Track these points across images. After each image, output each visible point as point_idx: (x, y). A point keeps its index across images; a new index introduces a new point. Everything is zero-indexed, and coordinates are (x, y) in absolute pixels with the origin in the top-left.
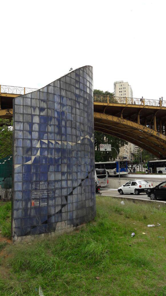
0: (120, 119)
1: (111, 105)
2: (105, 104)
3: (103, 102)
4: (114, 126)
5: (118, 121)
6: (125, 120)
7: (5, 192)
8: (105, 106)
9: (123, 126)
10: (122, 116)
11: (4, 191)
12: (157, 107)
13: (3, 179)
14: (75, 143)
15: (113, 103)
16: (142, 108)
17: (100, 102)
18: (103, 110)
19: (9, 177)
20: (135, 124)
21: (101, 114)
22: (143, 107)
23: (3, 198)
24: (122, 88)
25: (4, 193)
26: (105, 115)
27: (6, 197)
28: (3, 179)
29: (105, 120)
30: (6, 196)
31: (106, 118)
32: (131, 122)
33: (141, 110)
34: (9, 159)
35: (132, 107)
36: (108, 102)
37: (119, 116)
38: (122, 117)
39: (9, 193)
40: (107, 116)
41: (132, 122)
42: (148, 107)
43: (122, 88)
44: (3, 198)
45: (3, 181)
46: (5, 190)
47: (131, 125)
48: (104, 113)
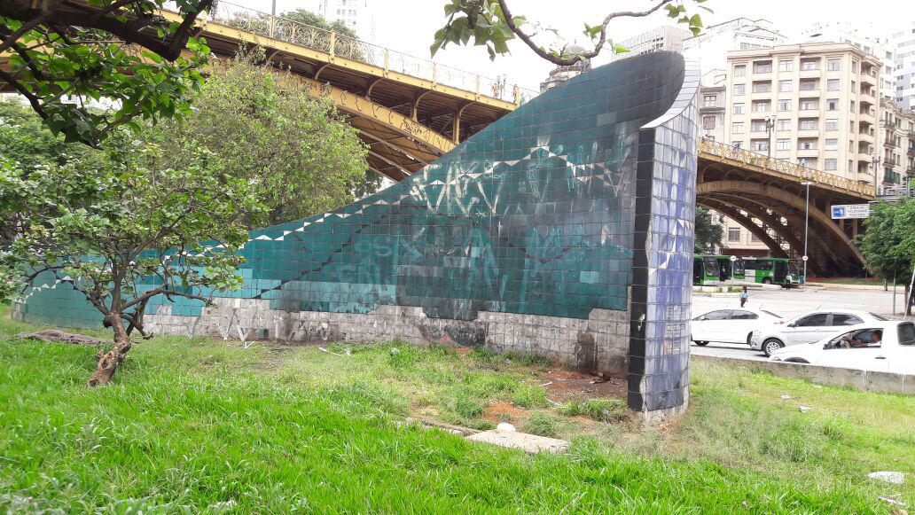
0: (409, 121)
1: (339, 62)
2: (323, 58)
3: (316, 48)
4: (388, 140)
5: (403, 128)
6: (423, 129)
7: (285, 319)
8: (321, 64)
9: (414, 146)
10: (415, 115)
11: (281, 318)
12: (508, 105)
13: (277, 283)
14: (655, 269)
15: (354, 59)
16: (470, 101)
17: (308, 47)
18: (314, 76)
19: (299, 279)
20: (448, 142)
21: (360, 101)
22: (473, 99)
23: (277, 336)
24: (347, 12)
25: (279, 323)
26: (370, 104)
27: (288, 332)
28: (277, 283)
29: (370, 120)
30: (288, 330)
31: (387, 122)
32: (437, 136)
33: (375, 84)
34: (301, 229)
35: (225, 37)
36: (332, 52)
37: (407, 115)
38: (415, 119)
39: (297, 324)
40: (376, 107)
41: (441, 138)
42: (397, 76)
43: (347, 12)
44: (277, 336)
45: (279, 288)
46: (284, 314)
47: (437, 145)
48: (368, 99)
